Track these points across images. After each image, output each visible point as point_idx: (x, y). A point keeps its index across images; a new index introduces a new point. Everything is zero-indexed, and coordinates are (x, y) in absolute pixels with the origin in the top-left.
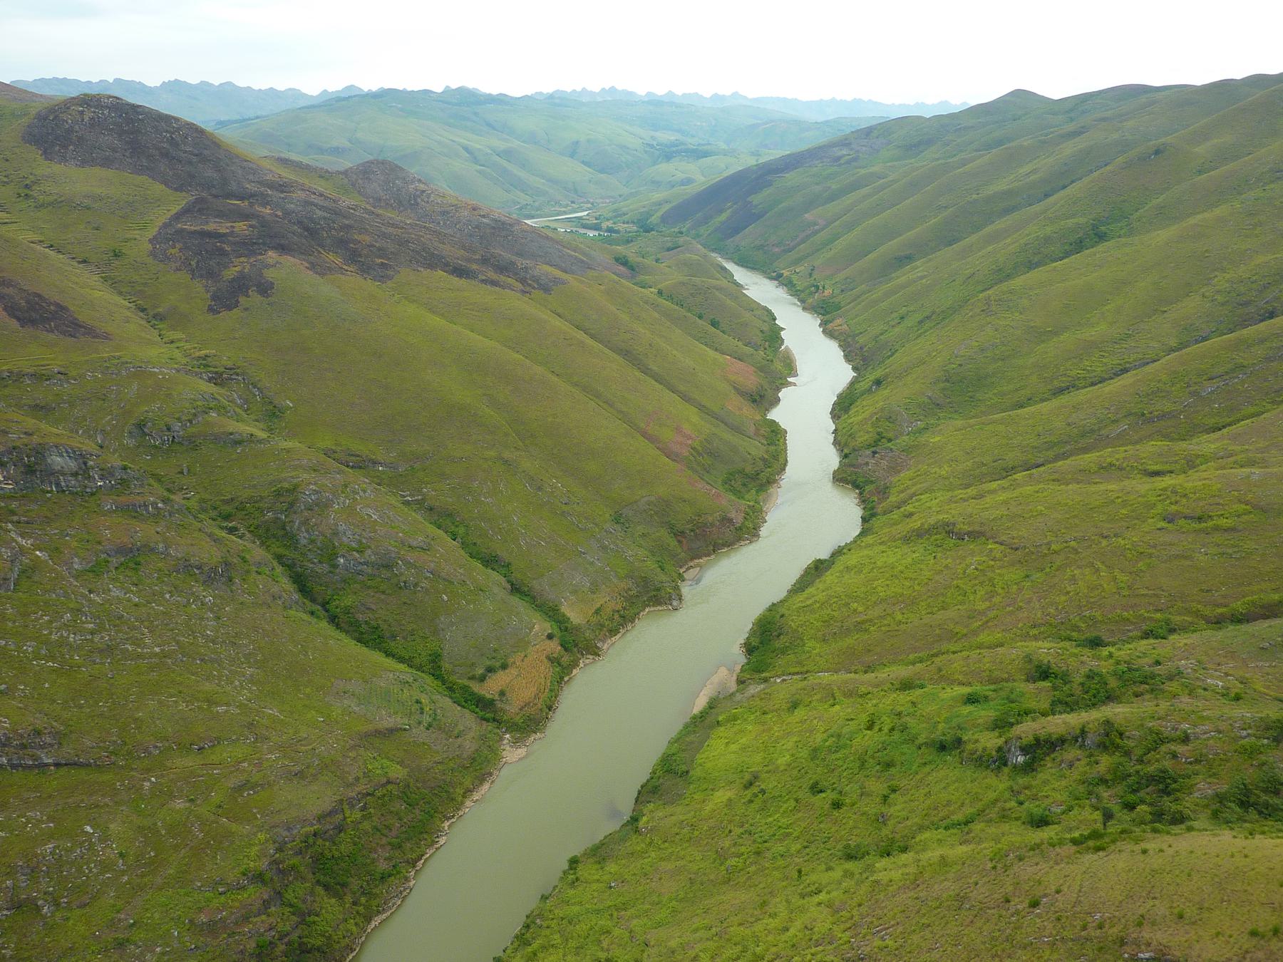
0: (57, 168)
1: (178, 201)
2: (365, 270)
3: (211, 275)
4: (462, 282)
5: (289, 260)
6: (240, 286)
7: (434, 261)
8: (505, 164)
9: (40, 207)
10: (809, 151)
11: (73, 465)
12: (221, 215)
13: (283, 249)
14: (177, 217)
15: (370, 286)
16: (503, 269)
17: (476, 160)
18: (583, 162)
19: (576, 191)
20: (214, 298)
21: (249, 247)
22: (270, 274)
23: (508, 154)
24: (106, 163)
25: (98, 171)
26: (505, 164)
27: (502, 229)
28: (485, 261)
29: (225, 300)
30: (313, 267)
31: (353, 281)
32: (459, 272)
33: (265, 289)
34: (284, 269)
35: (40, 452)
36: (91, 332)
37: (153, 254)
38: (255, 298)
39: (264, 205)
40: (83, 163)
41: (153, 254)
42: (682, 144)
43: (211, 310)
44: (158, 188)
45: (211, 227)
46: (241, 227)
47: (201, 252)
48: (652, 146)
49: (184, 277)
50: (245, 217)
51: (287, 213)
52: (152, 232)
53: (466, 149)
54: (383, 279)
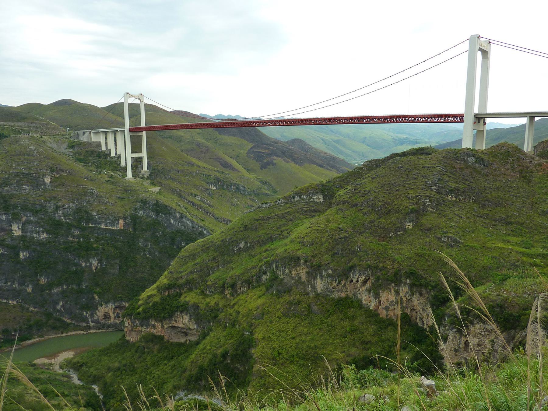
0: (223, 136)
1: (251, 145)
2: (296, 163)
3: (261, 161)
4: (321, 168)
5: (279, 158)
6: (268, 164)
7: (314, 163)
8: (336, 145)
9: (220, 145)
10: (455, 141)
11: (243, 189)
12: (262, 148)
13: (277, 156)
14: (252, 148)
15: (298, 167)
16: (332, 167)
17: (326, 144)
18: (367, 145)
19: (363, 156)
20: (262, 166)
21: (269, 155)
22: (275, 161)
23: (338, 142)
24: (234, 135)
25: (232, 137)
26: (336, 145)
27: (333, 159)
28: (327, 164)
29: (265, 166)
30: (284, 161)
31: (293, 164)
32: (320, 166)
33: (274, 164)
34: (278, 161)
35: (239, 185)
36: (237, 170)
37: (247, 156)
38: (271, 166)
39: (272, 146)
40: (229, 135)
41: (247, 156)
42: (409, 139)
43: (261, 169)
44: (246, 142)
45: (260, 150)
46: (267, 151)
47: (259, 157)
48: (395, 139)
49: (254, 161)
50: (268, 149)
51: (277, 149)
52: (246, 151)
53: (322, 139)
54: (301, 165)
